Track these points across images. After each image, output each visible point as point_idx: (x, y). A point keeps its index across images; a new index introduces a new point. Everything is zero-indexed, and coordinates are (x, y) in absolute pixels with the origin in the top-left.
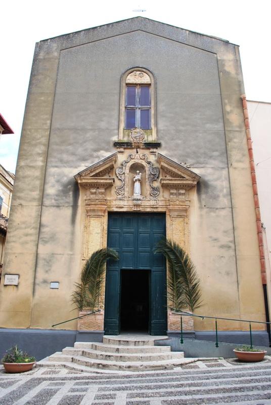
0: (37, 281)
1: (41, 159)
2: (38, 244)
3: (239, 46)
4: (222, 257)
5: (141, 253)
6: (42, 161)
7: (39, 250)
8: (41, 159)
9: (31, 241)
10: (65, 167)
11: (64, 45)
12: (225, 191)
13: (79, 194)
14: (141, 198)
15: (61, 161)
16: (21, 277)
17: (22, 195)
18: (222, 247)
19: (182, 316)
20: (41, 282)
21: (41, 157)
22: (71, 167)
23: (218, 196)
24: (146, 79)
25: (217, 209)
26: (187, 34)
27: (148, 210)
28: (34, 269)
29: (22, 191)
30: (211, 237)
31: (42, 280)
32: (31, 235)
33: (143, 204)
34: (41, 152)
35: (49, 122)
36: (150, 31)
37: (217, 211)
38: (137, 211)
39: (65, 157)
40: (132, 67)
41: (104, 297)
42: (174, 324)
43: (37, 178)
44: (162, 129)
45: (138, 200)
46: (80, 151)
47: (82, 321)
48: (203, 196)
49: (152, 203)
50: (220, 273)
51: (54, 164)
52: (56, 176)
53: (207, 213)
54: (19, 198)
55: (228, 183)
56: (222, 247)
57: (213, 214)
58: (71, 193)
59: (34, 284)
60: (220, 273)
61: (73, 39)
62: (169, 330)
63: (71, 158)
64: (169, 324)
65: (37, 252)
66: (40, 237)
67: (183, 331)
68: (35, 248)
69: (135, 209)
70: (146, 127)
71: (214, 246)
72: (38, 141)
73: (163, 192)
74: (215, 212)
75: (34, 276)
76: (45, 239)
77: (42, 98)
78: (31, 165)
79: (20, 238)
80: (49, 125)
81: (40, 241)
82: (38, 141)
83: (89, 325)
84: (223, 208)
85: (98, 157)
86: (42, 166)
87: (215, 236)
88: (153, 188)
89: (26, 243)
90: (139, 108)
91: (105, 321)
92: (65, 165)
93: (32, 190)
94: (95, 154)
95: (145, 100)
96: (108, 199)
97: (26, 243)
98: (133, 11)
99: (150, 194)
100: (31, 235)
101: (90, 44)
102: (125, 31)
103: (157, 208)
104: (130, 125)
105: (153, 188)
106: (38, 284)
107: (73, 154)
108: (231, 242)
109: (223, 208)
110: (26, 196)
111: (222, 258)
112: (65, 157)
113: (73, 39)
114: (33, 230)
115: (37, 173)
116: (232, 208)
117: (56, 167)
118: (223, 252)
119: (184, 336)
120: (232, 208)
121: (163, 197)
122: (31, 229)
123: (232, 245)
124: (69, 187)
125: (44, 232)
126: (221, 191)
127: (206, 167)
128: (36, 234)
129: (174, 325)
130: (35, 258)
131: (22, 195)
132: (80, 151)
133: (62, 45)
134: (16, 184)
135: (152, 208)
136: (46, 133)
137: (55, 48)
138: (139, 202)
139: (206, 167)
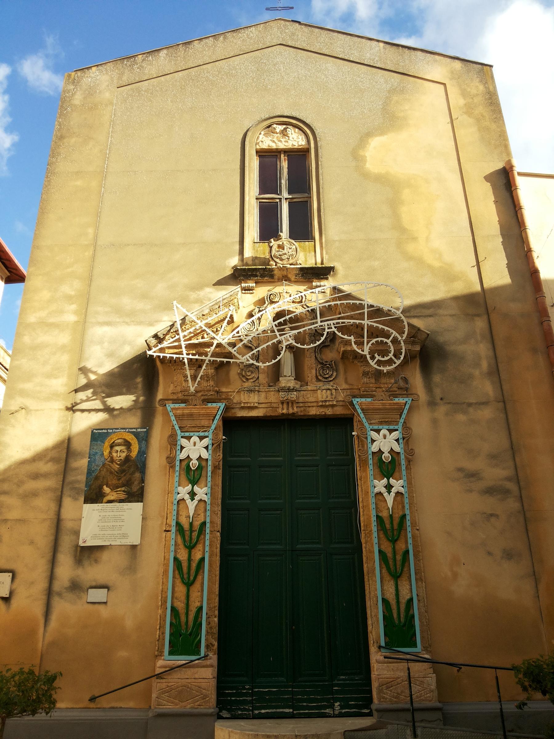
0: (57, 586)
1: (74, 307)
2: (61, 497)
3: (491, 66)
4: (492, 515)
5: (299, 469)
6: (75, 313)
7: (63, 511)
8: (74, 307)
9: (47, 490)
10: (127, 323)
11: (125, 78)
12: (485, 365)
13: (158, 382)
14: (298, 386)
15: (118, 311)
16: (17, 581)
17: (28, 386)
18: (490, 491)
19: (411, 665)
20: (66, 588)
21: (72, 304)
22: (140, 323)
23: (471, 377)
24: (295, 140)
25: (470, 405)
26: (382, 50)
27: (313, 411)
28: (49, 556)
29: (29, 377)
30: (460, 470)
31: (67, 584)
32: (45, 476)
33: (301, 400)
34: (73, 293)
35: (91, 231)
36: (304, 45)
37: (471, 410)
38: (288, 414)
39: (126, 302)
40: (267, 116)
41: (216, 620)
42: (387, 684)
43: (63, 348)
44: (336, 238)
45: (289, 390)
46: (160, 289)
47: (162, 684)
48: (437, 378)
49: (322, 395)
50: (489, 553)
51: (101, 319)
52: (106, 344)
53: (447, 414)
54: (23, 393)
55: (490, 346)
56: (490, 491)
57: (461, 417)
58: (139, 380)
59: (49, 593)
60: (489, 553)
61: (144, 64)
62: (375, 700)
63: (140, 305)
64: (375, 685)
65: (58, 514)
66: (67, 480)
67: (416, 705)
68: (53, 506)
69: (285, 411)
70: (302, 230)
71: (471, 491)
72: (69, 270)
73: (345, 372)
74: (465, 412)
75: (49, 574)
76: (77, 486)
77: (79, 183)
78: (52, 320)
79: (20, 483)
80: (91, 236)
81: (67, 492)
82: (69, 270)
83: (182, 693)
84: (483, 403)
85: (199, 301)
86: (76, 322)
87: (470, 465)
88: (322, 363)
89: (34, 494)
90: (286, 199)
91: (218, 682)
92: (127, 320)
93: (50, 376)
94: (193, 296)
95: (301, 181)
96: (224, 390)
97: (34, 494)
98: (292, 8)
99: (317, 377)
100: (45, 476)
101: (180, 74)
102: (251, 48)
103: (333, 406)
104: (269, 231)
105: (322, 363)
106: (59, 594)
107: (144, 296)
108: (509, 479)
109: (483, 403)
110: (38, 388)
111: (493, 519)
112: (126, 302)
113: (144, 64)
114: (50, 464)
115: (64, 338)
116: (504, 402)
117: (108, 324)
118: (490, 504)
119: (418, 716)
120: (504, 402)
121: (346, 382)
122: (47, 463)
123: (511, 486)
124: (135, 366)
125: (76, 469)
126: (477, 365)
127: (436, 315)
128: (57, 475)
129: (387, 688)
130: (53, 531)
131: (28, 386)
132: (160, 289)
133: (120, 78)
134: (16, 363)
135: (322, 406)
136: (87, 254)
137: (107, 84)
138: (293, 396)
139: (436, 315)
